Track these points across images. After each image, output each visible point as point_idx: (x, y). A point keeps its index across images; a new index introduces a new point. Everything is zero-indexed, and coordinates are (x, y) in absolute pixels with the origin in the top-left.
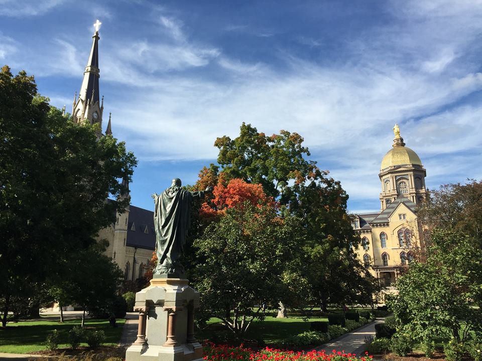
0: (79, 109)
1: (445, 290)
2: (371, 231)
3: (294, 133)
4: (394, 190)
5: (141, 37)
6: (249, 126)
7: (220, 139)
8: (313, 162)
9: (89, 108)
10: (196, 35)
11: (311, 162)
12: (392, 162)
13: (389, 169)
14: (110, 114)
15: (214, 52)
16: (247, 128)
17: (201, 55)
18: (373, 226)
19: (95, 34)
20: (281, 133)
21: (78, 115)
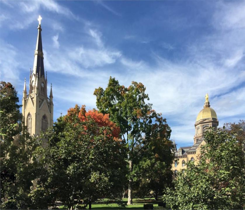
0: (33, 81)
1: (206, 185)
2: (187, 157)
3: (140, 83)
4: (201, 133)
6: (114, 79)
8: (150, 104)
10: (109, 42)
11: (149, 104)
12: (202, 117)
13: (201, 121)
15: (118, 54)
16: (112, 80)
18: (188, 154)
19: (39, 27)
20: (132, 84)
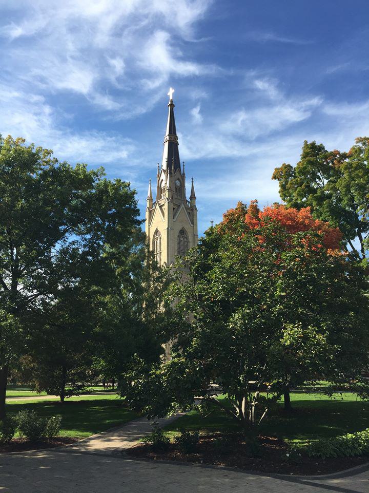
0: (162, 180)
5: (238, 108)
7: (278, 169)
9: (170, 177)
14: (192, 178)
15: (315, 101)
17: (302, 107)
21: (162, 186)
